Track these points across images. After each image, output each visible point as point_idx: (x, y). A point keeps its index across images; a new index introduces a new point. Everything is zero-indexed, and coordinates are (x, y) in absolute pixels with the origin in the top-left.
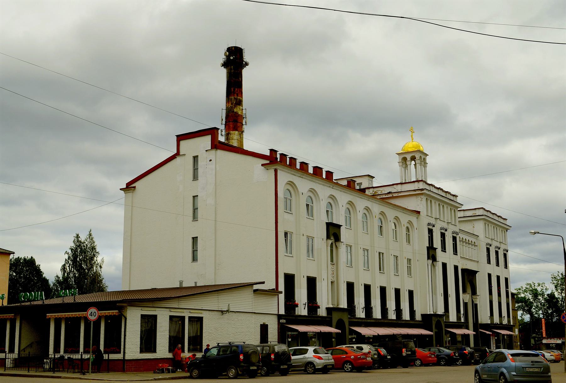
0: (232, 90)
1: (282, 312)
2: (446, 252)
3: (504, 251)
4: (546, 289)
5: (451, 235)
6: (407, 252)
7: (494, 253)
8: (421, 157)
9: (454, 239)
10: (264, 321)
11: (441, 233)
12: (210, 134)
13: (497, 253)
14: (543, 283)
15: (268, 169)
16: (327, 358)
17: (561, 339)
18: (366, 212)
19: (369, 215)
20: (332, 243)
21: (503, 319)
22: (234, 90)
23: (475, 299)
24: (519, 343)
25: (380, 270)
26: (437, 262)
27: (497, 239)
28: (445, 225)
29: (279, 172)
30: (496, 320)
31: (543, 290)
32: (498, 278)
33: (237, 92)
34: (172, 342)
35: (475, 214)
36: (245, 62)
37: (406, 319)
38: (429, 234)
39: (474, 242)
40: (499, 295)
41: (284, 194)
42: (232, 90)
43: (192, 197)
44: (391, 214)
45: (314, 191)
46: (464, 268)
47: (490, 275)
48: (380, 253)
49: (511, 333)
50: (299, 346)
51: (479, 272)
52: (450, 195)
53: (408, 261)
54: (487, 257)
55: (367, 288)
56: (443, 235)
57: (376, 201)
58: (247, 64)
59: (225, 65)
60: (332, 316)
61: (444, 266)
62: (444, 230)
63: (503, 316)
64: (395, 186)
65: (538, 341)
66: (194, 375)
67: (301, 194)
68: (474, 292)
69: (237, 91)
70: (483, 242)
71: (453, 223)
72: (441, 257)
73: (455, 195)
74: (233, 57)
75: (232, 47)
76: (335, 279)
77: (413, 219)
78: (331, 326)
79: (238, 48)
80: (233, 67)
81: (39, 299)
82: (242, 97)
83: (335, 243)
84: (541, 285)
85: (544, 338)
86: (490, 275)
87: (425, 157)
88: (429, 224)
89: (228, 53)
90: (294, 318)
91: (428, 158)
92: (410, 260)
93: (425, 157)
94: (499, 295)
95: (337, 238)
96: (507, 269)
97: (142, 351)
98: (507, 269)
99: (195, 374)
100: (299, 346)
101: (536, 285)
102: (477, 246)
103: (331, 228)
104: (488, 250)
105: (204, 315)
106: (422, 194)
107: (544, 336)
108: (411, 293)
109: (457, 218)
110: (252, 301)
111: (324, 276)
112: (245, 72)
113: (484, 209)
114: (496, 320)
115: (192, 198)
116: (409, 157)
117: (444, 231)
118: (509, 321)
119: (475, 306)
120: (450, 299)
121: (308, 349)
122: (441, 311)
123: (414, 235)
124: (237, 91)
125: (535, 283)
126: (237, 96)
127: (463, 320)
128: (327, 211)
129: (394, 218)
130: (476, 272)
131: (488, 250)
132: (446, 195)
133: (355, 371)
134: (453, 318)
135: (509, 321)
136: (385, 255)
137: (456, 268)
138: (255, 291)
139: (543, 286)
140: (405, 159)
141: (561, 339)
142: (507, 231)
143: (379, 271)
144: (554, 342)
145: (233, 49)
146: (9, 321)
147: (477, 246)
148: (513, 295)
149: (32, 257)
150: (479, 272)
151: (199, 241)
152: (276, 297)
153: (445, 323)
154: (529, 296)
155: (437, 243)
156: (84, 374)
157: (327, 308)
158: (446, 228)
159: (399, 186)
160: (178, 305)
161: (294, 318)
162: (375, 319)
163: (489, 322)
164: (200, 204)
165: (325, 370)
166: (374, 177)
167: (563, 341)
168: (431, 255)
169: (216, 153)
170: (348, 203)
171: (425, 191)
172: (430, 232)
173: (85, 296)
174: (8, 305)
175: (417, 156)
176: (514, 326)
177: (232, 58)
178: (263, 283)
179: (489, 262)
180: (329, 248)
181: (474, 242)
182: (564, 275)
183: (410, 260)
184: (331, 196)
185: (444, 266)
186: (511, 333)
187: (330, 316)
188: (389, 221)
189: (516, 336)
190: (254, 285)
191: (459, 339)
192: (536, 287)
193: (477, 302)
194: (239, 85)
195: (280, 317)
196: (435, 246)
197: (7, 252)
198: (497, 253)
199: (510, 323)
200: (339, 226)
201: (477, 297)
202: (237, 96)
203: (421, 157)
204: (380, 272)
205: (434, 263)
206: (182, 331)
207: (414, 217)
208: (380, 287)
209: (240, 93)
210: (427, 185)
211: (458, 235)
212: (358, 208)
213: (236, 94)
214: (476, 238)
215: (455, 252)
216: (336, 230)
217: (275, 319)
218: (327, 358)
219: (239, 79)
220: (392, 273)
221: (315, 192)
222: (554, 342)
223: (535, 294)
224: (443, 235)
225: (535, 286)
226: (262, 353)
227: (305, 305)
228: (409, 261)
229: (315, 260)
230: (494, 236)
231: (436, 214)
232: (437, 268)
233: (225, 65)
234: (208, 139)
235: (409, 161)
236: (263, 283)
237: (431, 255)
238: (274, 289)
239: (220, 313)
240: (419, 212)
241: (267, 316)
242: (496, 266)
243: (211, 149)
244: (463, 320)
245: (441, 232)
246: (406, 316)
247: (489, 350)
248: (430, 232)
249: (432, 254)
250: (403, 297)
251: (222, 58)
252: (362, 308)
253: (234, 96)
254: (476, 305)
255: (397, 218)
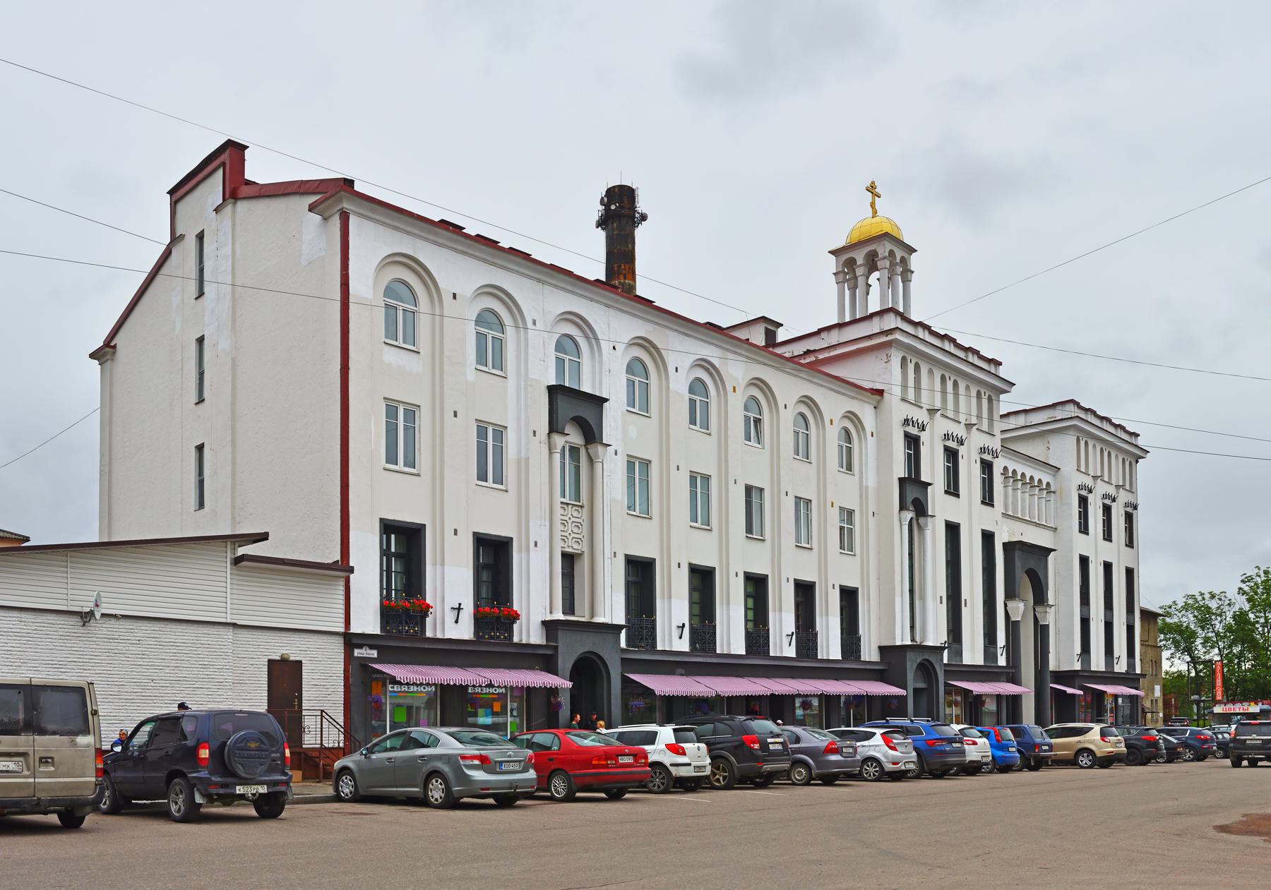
0: (616, 269)
1: (1228, 762)
2: (993, 506)
3: (1243, 581)
4: (1229, 605)
5: (976, 456)
6: (844, 490)
7: (1100, 512)
8: (892, 253)
9: (987, 467)
10: (284, 652)
11: (947, 449)
12: (881, 659)
13: (1107, 510)
14: (1221, 593)
15: (300, 553)
16: (1116, 744)
17: (1260, 704)
18: (638, 352)
19: (857, 430)
20: (912, 519)
21: (1115, 661)
22: (956, 704)
23: (1042, 614)
24: (1161, 715)
25: (749, 529)
26: (929, 519)
27: (957, 411)
28: (1111, 490)
29: (353, 221)
30: (1098, 662)
31: (1222, 607)
32: (1108, 567)
33: (624, 272)
34: (219, 779)
35: (1052, 418)
36: (639, 213)
37: (732, 653)
38: (1080, 507)
39: (1048, 484)
40: (1109, 626)
41: (444, 776)
42: (616, 269)
43: (194, 341)
44: (833, 405)
45: (811, 403)
46: (382, 517)
47: (1084, 561)
48: (749, 489)
49: (1134, 692)
50: (1077, 721)
51: (1055, 550)
52: (929, 333)
53: (645, 460)
54: (1104, 526)
55: (805, 591)
56: (952, 456)
57: (735, 346)
58: (644, 217)
59: (602, 223)
60: (557, 643)
61: (953, 530)
62: (953, 441)
63: (1116, 655)
64: (824, 335)
65: (1204, 708)
66: (795, 778)
67: (447, 298)
68: (1040, 598)
69: (625, 269)
70: (1073, 480)
71: (985, 428)
72: (941, 507)
73: (1119, 425)
74: (616, 206)
75: (614, 187)
76: (584, 547)
77: (866, 413)
78: (1075, 688)
79: (626, 188)
80: (617, 226)
81: (357, 652)
82: (634, 279)
83: (587, 449)
84: (1217, 597)
85: (1220, 702)
86: (1084, 561)
87: (906, 255)
88: (906, 422)
89: (606, 199)
90: (393, 596)
91: (1076, 468)
92: (850, 513)
93: (906, 255)
94: (1109, 626)
95: (592, 434)
96: (1132, 547)
97: (1005, 545)
98: (1132, 547)
99: (105, 804)
100: (843, 699)
101: (1207, 596)
102: (1054, 492)
103: (564, 406)
104: (1083, 501)
105: (784, 634)
106: (888, 345)
107: (1219, 698)
108: (849, 597)
109: (996, 417)
110: (224, 600)
111: (539, 531)
112: (642, 234)
113: (1077, 404)
114: (1098, 662)
115: (193, 454)
116: (860, 255)
117: (1087, 491)
118: (1131, 665)
119: (1042, 632)
120: (965, 612)
121: (657, 732)
122: (936, 634)
123: (866, 451)
124: (625, 269)
125: (1204, 594)
126: (625, 278)
127: (1002, 661)
128: (842, 528)
129: (845, 417)
130: (1048, 551)
131: (1083, 501)
132: (1117, 432)
133: (603, 795)
134: (973, 654)
135: (1131, 665)
136: (767, 494)
137: (988, 537)
138: (237, 561)
139: (1223, 599)
140: (851, 263)
141: (1260, 704)
142: (1137, 462)
143: (745, 534)
144: (1241, 709)
145: (616, 190)
146: (828, 756)
147: (1054, 492)
148: (1148, 616)
149: (644, 217)
150: (1055, 550)
151: (206, 450)
152: (339, 583)
153: (947, 669)
154: (1189, 619)
155: (933, 469)
156: (706, 714)
157: (544, 623)
158: (1090, 486)
159: (835, 333)
160: (65, 575)
161: (393, 596)
162: (822, 661)
163: (1077, 666)
164: (192, 288)
165: (1106, 762)
166: (782, 325)
167: (1265, 707)
168: (909, 499)
169: (1025, 417)
170: (845, 417)
171: (898, 336)
172: (913, 442)
173: (99, 689)
174: (1049, 674)
175: (883, 249)
176: (1143, 675)
177: (613, 207)
178: (263, 537)
179: (1084, 529)
180: (906, 528)
181: (1048, 484)
182: (1168, 620)
183: (850, 513)
184: (848, 414)
185: (953, 530)
186: (1134, 692)
187: (554, 644)
188: (729, 389)
189: (1156, 700)
190: (531, 376)
191: (991, 706)
192: (1207, 603)
193: (1050, 618)
194: (630, 258)
195: (351, 641)
196: (924, 477)
197: (8, 535)
198: (1107, 510)
199: (1134, 669)
200: (599, 401)
201: (1048, 609)
202: (625, 278)
203: (892, 253)
204: (749, 536)
205: (921, 520)
206: (1007, 646)
207: (866, 405)
208: (1104, 563)
209: (631, 274)
210: (1080, 411)
211: (997, 457)
212: (671, 360)
213: (622, 276)
214: (1053, 473)
215: (988, 500)
216: (586, 413)
217: (336, 648)
218: (903, 754)
219: (628, 247)
220: (788, 539)
221: (768, 389)
222: (1241, 709)
223: (1205, 616)
224: (952, 456)
225: (1204, 599)
226: (1188, 677)
227: (456, 612)
228: (848, 514)
229: (421, 351)
230: (944, 400)
231: (1094, 468)
232: (928, 533)
233: (602, 223)
234: (214, 188)
235: (860, 266)
236: (263, 537)
237: (909, 499)
238: (338, 561)
239: (75, 620)
240: (880, 392)
241: (296, 637)
242: (983, 503)
243: (224, 199)
244: (1002, 661)
245: (944, 445)
246: (830, 647)
247: (477, 328)
248: (913, 442)
249: (901, 255)
250: (866, 613)
251: (596, 210)
252: (679, 627)
253: (619, 278)
254: (1045, 629)
255: (851, 416)
